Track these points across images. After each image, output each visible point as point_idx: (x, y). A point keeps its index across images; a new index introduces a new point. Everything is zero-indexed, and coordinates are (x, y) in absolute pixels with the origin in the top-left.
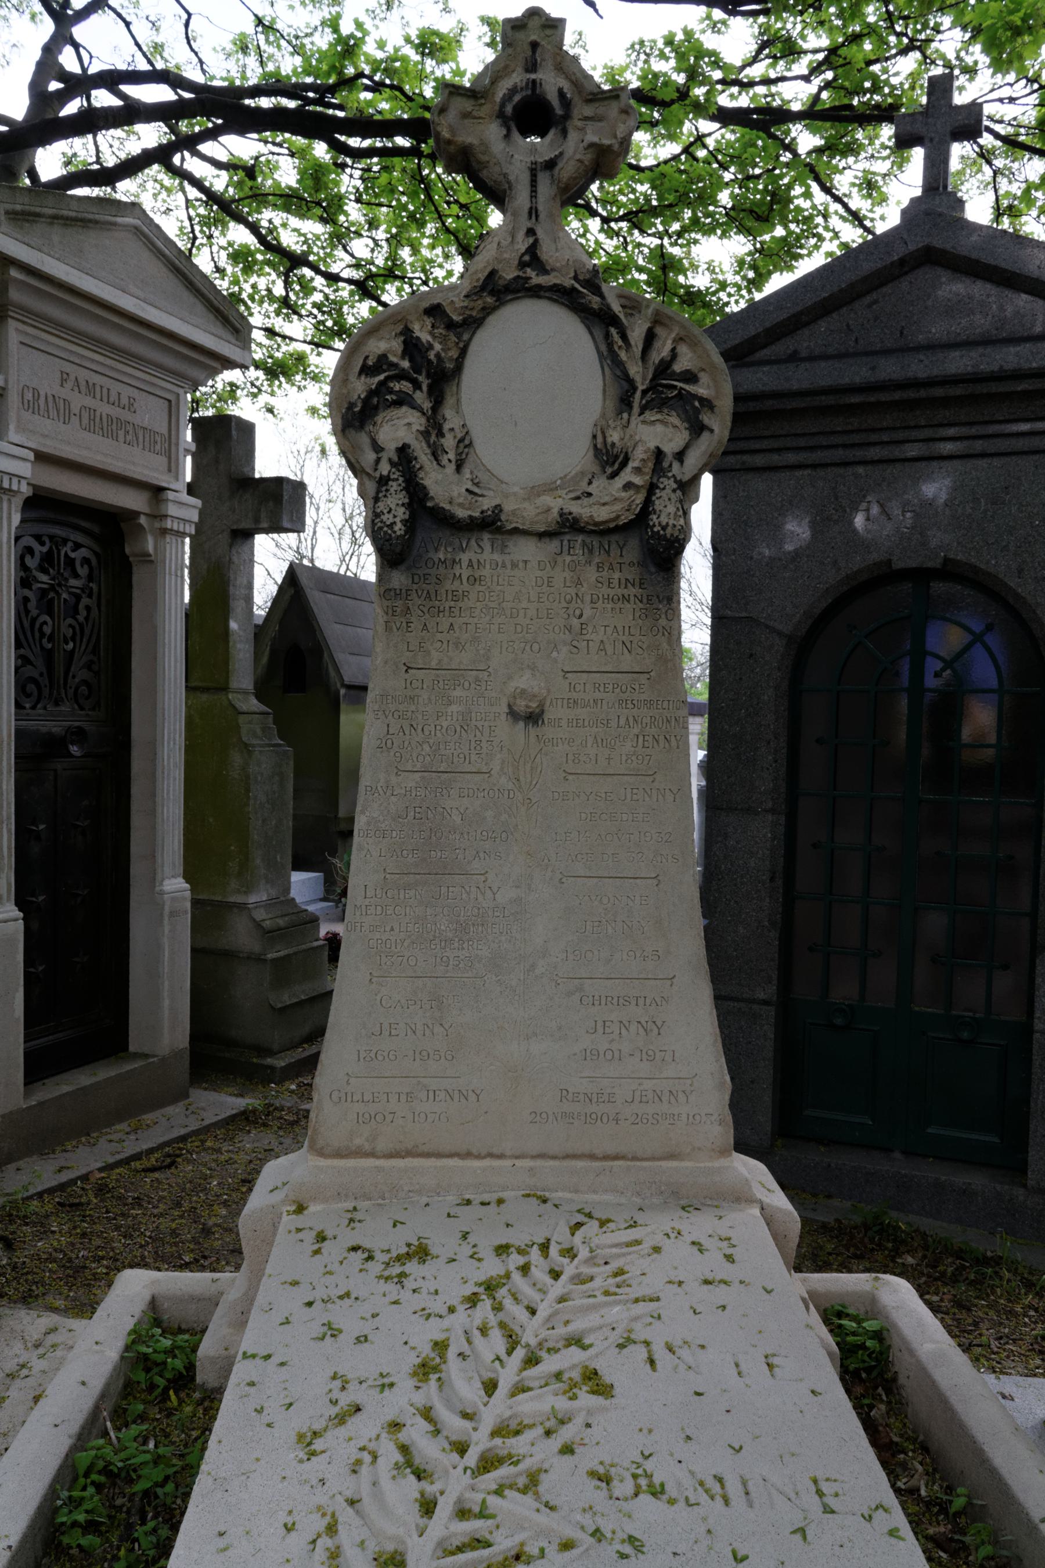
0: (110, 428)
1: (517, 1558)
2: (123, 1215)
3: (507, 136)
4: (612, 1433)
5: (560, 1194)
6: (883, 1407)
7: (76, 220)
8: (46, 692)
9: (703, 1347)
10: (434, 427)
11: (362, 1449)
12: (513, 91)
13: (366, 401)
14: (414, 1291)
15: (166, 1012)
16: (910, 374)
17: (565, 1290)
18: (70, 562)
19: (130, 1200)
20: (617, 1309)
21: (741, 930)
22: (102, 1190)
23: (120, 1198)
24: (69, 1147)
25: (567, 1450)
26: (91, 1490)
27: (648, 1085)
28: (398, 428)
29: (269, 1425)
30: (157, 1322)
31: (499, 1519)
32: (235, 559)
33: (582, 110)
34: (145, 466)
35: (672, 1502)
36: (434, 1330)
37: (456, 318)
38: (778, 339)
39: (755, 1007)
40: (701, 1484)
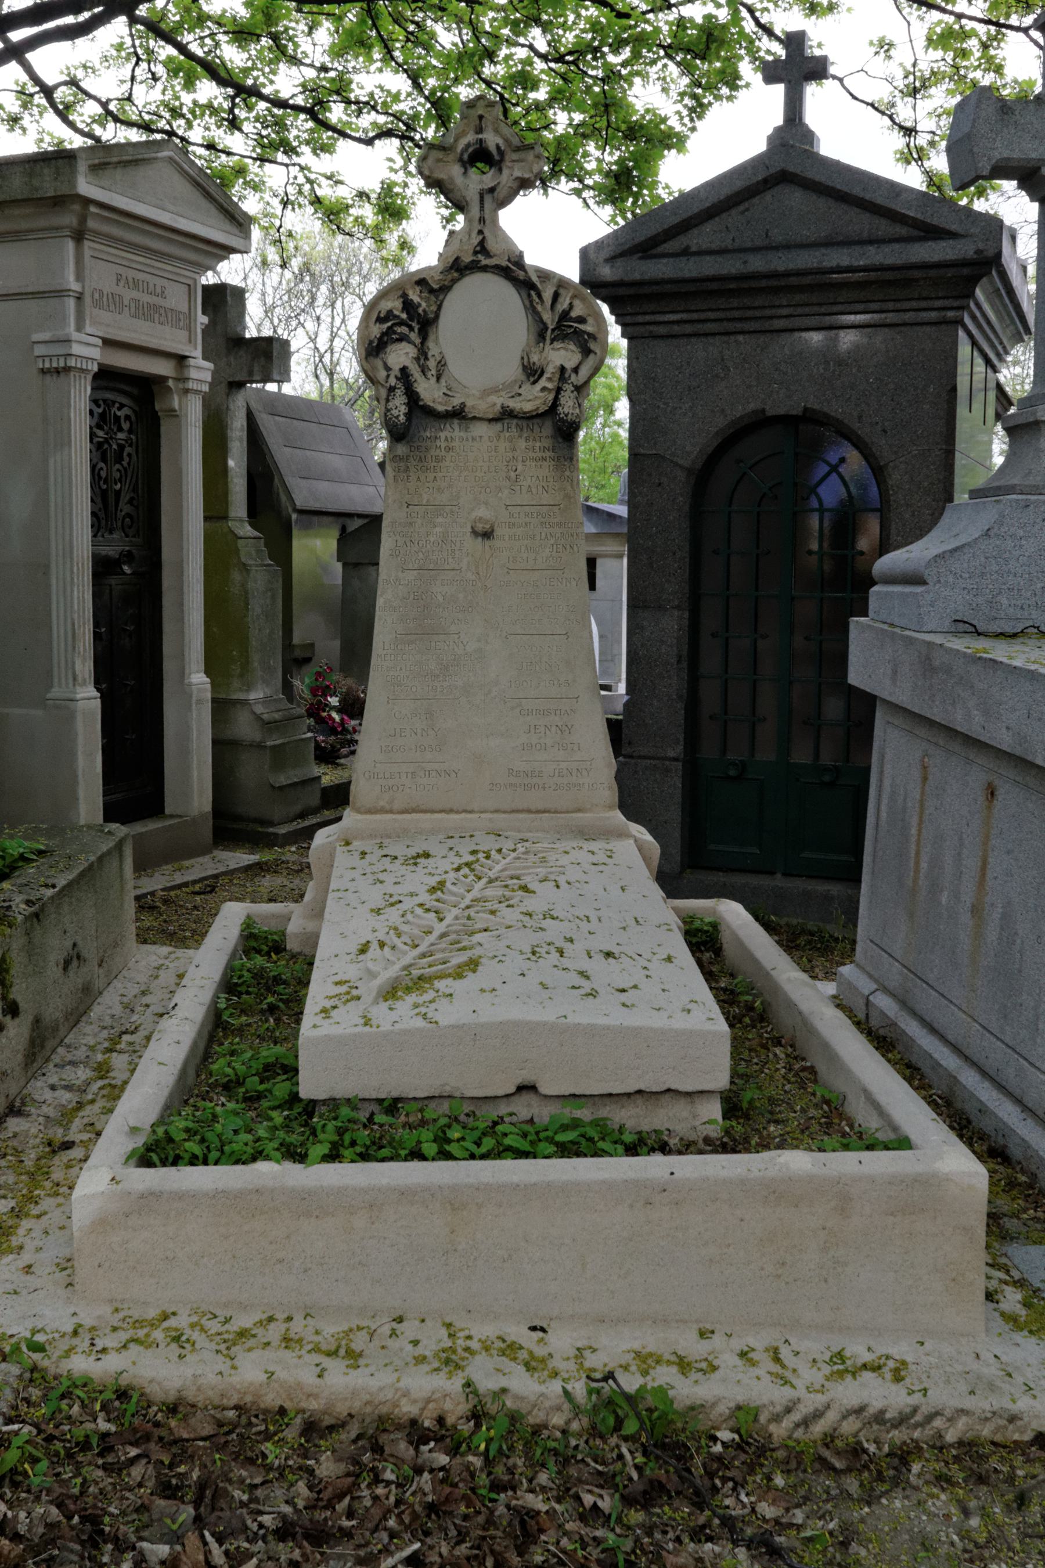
0: (148, 312)
3: (465, 173)
7: (130, 162)
8: (103, 522)
10: (423, 354)
12: (468, 145)
13: (380, 339)
15: (195, 779)
16: (772, 267)
18: (117, 419)
21: (655, 703)
22: (166, 901)
27: (563, 765)
28: (400, 355)
32: (231, 407)
33: (510, 156)
34: (173, 340)
37: (435, 287)
38: (674, 237)
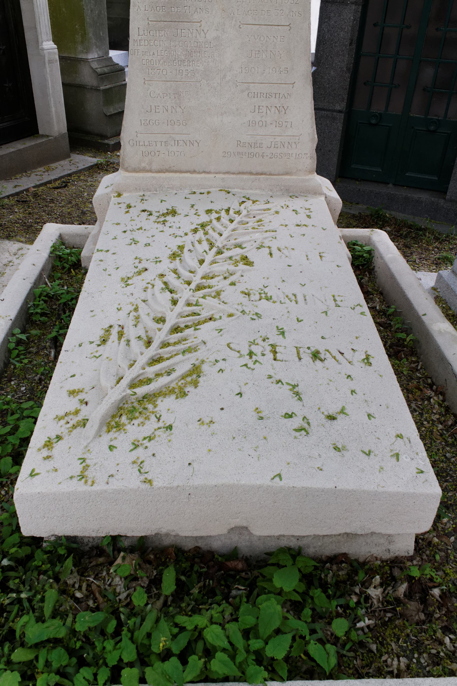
1: (210, 319)
2: (46, 206)
4: (252, 279)
5: (236, 190)
6: (367, 278)
9: (293, 249)
11: (148, 283)
14: (170, 227)
17: (236, 227)
19: (49, 200)
20: (257, 234)
21: (332, 73)
23: (44, 199)
24: (18, 177)
25: (233, 284)
26: (42, 302)
27: (278, 139)
29: (109, 275)
30: (63, 244)
31: (203, 306)
35: (274, 302)
36: (179, 241)
39: (335, 113)
40: (287, 296)
